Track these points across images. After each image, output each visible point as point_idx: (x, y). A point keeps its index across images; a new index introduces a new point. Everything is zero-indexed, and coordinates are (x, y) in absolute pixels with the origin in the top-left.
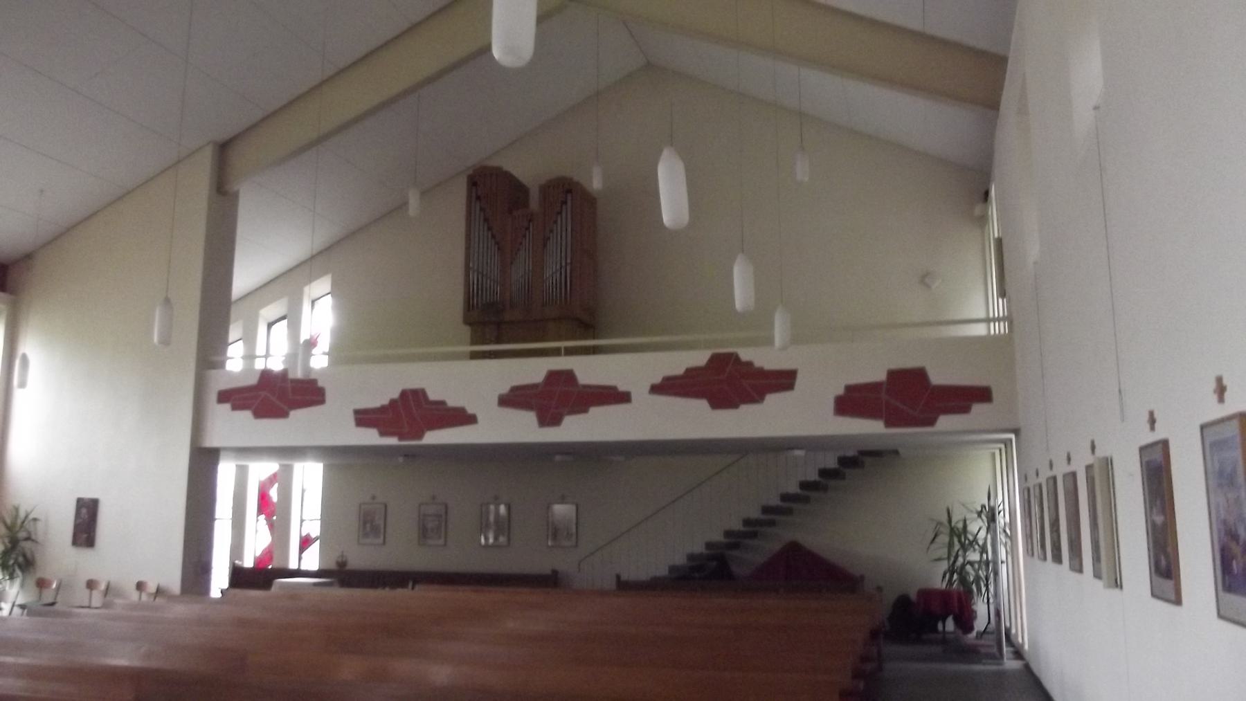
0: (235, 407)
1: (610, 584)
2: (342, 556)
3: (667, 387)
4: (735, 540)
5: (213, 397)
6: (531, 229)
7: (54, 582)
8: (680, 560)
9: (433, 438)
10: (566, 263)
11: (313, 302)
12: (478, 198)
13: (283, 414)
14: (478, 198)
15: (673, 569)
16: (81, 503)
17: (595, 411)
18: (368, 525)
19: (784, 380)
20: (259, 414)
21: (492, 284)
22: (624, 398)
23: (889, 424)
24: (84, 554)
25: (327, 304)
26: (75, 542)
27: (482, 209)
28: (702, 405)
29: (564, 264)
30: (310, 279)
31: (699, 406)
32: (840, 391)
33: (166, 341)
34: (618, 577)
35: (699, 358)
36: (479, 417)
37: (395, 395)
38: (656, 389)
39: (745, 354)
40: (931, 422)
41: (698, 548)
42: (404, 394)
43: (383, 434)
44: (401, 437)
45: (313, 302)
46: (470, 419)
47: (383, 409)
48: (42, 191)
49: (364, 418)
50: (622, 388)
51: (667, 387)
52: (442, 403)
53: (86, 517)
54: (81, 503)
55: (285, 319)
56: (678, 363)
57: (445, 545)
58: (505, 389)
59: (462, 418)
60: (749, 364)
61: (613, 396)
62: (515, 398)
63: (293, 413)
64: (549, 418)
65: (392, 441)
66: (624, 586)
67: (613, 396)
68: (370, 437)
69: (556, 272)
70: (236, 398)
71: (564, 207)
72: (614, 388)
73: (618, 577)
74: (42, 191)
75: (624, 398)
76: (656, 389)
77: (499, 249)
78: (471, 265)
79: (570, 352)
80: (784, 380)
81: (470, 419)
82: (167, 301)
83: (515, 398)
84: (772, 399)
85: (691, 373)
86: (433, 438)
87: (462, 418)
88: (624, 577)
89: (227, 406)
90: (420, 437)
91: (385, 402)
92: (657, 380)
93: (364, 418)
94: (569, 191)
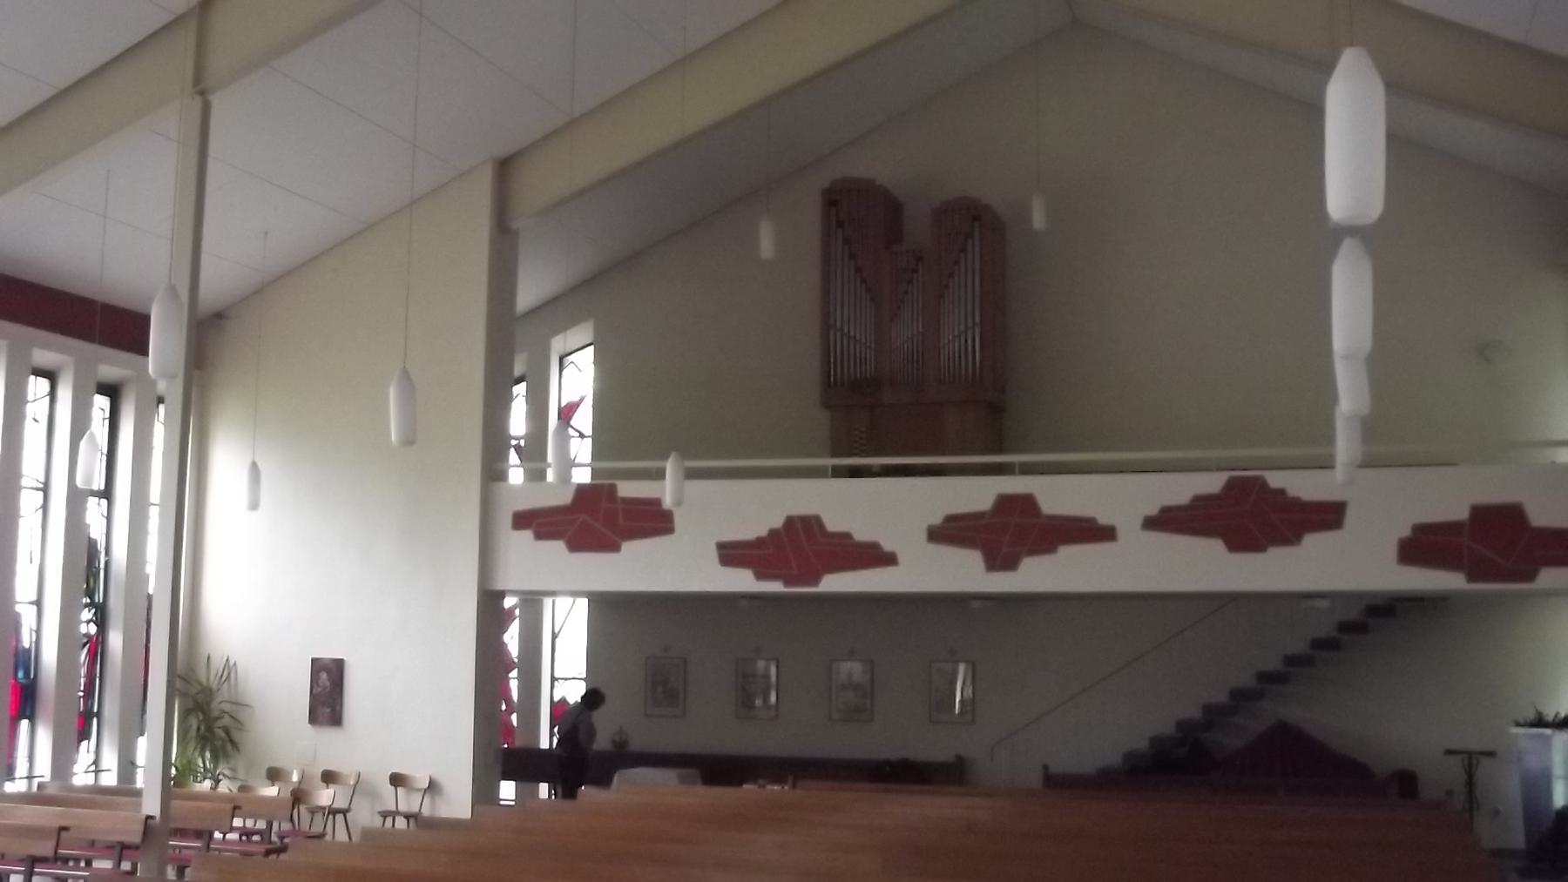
0: (540, 536)
1: (1035, 780)
2: (621, 731)
3: (1166, 521)
4: (1214, 715)
5: (506, 520)
6: (920, 271)
7: (293, 772)
8: (1140, 743)
9: (835, 583)
10: (974, 324)
11: (561, 359)
12: (840, 224)
13: (613, 547)
14: (840, 224)
15: (1130, 757)
16: (317, 666)
17: (1068, 553)
18: (660, 689)
19: (1328, 516)
20: (576, 546)
21: (852, 347)
22: (1103, 534)
23: (1472, 578)
24: (328, 735)
25: (585, 360)
26: (314, 719)
27: (846, 241)
28: (1216, 546)
29: (970, 325)
30: (563, 328)
31: (1213, 548)
32: (1406, 532)
33: (409, 440)
34: (1046, 767)
35: (1212, 483)
36: (901, 558)
37: (778, 522)
38: (1152, 523)
39: (1275, 479)
40: (1530, 576)
41: (1166, 728)
42: (790, 522)
43: (760, 576)
44: (787, 583)
45: (561, 359)
46: (889, 559)
47: (759, 543)
48: (266, 233)
49: (731, 554)
50: (1103, 519)
51: (1166, 521)
52: (847, 536)
53: (328, 684)
54: (317, 666)
55: (523, 381)
56: (1181, 489)
57: (777, 716)
58: (936, 519)
59: (875, 556)
60: (1282, 492)
61: (1091, 532)
62: (951, 532)
63: (629, 547)
64: (1000, 560)
65: (775, 587)
66: (1054, 781)
67: (1091, 532)
68: (742, 581)
69: (959, 336)
70: (540, 523)
71: (970, 242)
72: (1091, 521)
73: (1046, 767)
74: (266, 233)
75: (1103, 534)
76: (1152, 523)
77: (872, 299)
78: (832, 322)
79: (1027, 470)
80: (1328, 516)
81: (889, 559)
82: (406, 375)
83: (951, 532)
84: (1312, 541)
85: (1200, 502)
86: (835, 583)
87: (875, 556)
88: (1057, 767)
89: (527, 535)
90: (815, 580)
91: (763, 532)
92: (1153, 510)
93: (731, 554)
94: (976, 218)
